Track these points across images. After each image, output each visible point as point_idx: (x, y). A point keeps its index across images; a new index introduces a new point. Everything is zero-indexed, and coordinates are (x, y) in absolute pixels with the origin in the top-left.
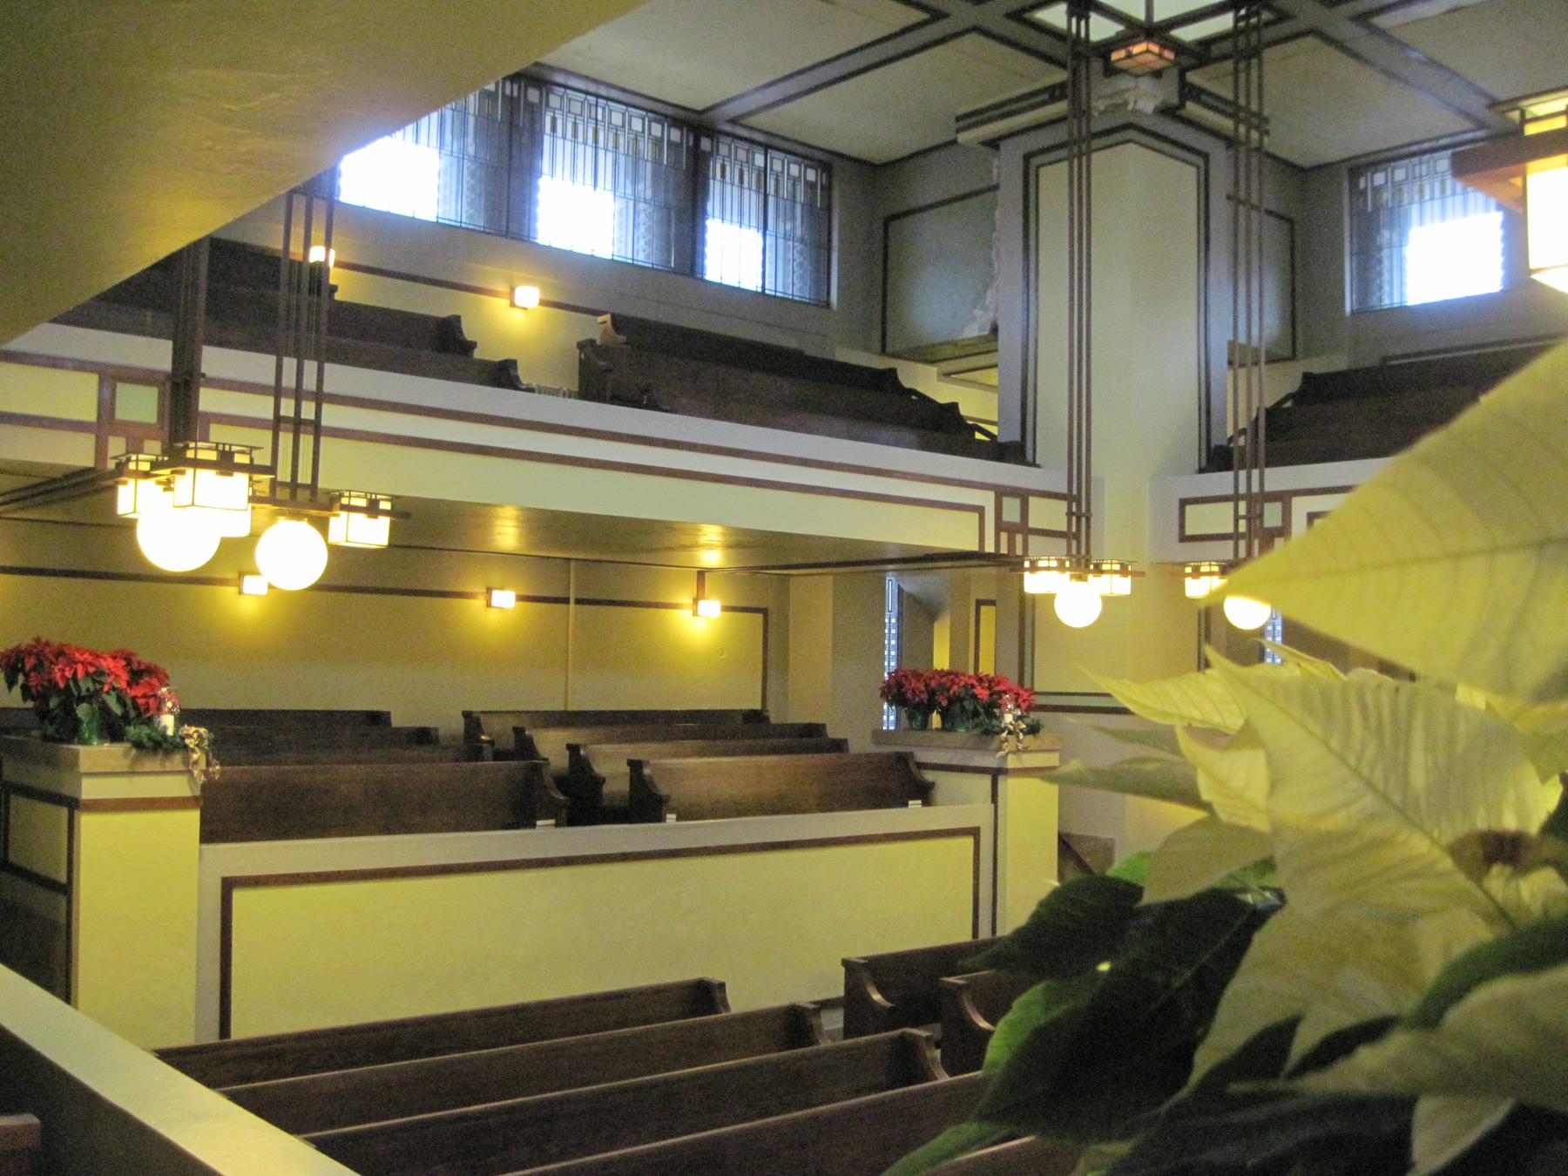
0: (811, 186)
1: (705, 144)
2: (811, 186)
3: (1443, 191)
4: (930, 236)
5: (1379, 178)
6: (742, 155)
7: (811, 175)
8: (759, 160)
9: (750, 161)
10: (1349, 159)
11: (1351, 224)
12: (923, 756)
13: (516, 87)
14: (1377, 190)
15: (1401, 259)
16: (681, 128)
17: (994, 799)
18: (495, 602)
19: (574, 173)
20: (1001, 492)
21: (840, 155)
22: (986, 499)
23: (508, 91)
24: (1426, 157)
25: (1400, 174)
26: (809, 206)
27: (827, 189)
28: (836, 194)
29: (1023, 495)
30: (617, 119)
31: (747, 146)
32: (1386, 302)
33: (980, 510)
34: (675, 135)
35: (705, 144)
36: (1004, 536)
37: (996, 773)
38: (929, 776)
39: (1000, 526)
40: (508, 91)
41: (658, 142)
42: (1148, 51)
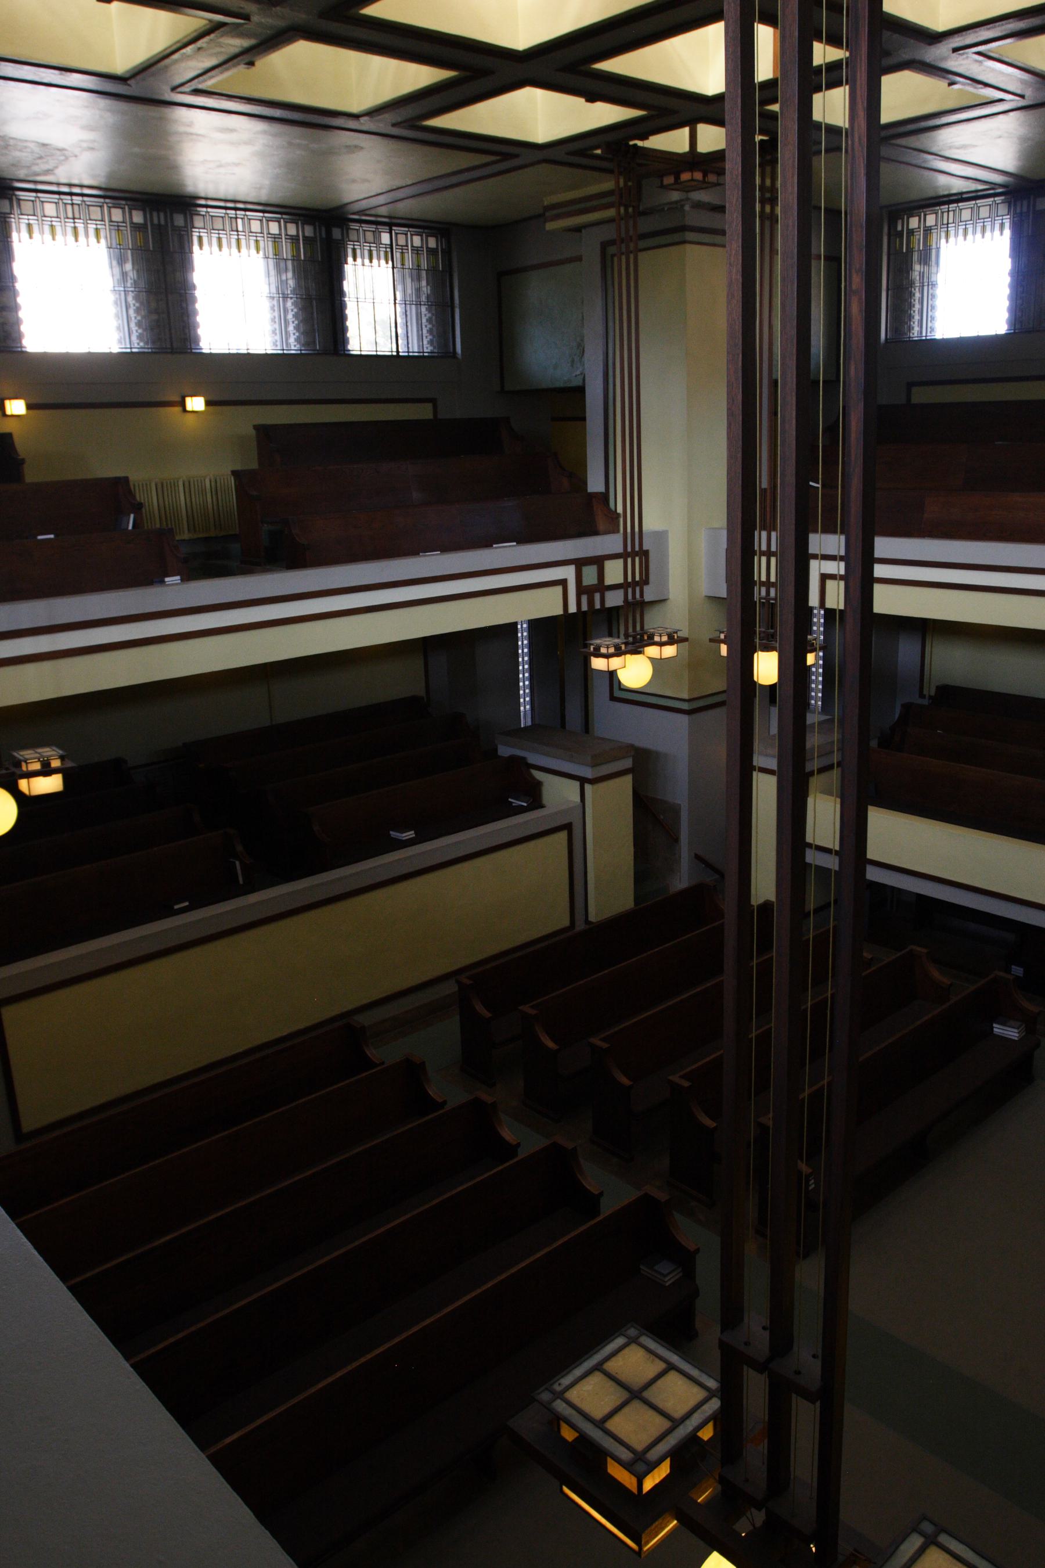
0: (432, 252)
1: (336, 233)
2: (432, 252)
3: (966, 230)
4: (537, 292)
5: (914, 223)
6: (370, 236)
7: (432, 243)
8: (385, 238)
9: (377, 241)
10: (891, 206)
11: (1002, 73)
12: (533, 758)
13: (162, 215)
14: (911, 232)
15: (1019, 159)
16: (314, 225)
18: (189, 408)
19: (220, 246)
20: (580, 563)
21: (455, 225)
22: (568, 572)
23: (156, 221)
24: (952, 206)
25: (931, 220)
26: (432, 271)
27: (447, 253)
28: (454, 255)
29: (598, 561)
30: (256, 226)
31: (373, 228)
32: (915, 334)
33: (563, 583)
34: (309, 231)
35: (336, 233)
36: (584, 599)
38: (538, 775)
39: (581, 590)
40: (156, 221)
41: (294, 239)
42: (692, 180)
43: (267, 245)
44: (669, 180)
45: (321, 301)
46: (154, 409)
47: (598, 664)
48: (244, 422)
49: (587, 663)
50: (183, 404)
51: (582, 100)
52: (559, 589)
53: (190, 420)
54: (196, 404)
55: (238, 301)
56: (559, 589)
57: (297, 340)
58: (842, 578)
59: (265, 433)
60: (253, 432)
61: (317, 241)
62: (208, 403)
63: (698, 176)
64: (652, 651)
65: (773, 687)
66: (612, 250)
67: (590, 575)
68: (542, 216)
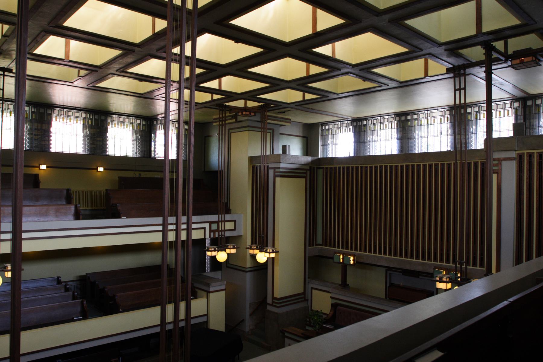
17: (207, 298)
20: (211, 223)
22: (207, 226)
33: (204, 228)
36: (212, 234)
37: (208, 292)
38: (197, 290)
39: (211, 231)
43: (135, 126)
44: (240, 114)
45: (97, 135)
46: (88, 170)
47: (209, 253)
48: (116, 175)
49: (205, 254)
50: (97, 169)
51: (362, 80)
52: (203, 230)
53: (99, 174)
54: (101, 169)
55: (121, 141)
56: (203, 230)
57: (471, 137)
58: (175, 230)
59: (121, 178)
60: (117, 179)
61: (146, 126)
62: (104, 169)
63: (248, 113)
64: (228, 251)
65: (221, 263)
66: (231, 131)
67: (214, 227)
68: (213, 122)
